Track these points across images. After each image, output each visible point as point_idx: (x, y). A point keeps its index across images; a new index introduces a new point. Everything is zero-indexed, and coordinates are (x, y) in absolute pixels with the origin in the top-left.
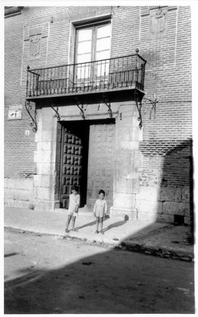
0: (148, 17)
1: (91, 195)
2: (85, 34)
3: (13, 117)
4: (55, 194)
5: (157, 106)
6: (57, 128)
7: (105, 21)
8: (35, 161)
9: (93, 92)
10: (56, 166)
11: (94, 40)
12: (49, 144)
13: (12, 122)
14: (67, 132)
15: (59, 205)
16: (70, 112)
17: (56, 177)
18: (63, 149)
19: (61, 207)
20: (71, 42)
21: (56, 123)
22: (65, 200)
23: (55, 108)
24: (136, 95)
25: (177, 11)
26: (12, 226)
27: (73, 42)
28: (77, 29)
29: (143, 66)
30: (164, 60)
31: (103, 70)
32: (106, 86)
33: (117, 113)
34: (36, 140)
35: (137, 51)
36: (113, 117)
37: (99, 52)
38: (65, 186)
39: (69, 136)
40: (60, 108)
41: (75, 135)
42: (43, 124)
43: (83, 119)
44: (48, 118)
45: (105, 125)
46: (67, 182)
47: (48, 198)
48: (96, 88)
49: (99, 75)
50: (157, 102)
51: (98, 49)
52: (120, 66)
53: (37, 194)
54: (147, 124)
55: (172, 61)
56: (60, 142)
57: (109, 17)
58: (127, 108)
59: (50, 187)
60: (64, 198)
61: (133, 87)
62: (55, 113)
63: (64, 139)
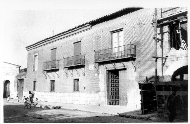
0: (136, 28)
1: (120, 99)
2: (115, 35)
3: (91, 69)
4: (107, 99)
5: (141, 63)
6: (107, 72)
7: (121, 30)
8: (99, 86)
9: (116, 59)
10: (107, 88)
11: (118, 37)
12: (104, 79)
13: (90, 71)
14: (111, 74)
15: (109, 104)
16: (111, 67)
17: (107, 92)
18: (110, 81)
19: (110, 104)
20: (110, 39)
21: (106, 71)
22: (112, 102)
23: (123, 63)
24: (132, 59)
25: (146, 25)
26: (87, 110)
27: (111, 38)
28: (112, 33)
29: (135, 47)
30: (142, 45)
31: (122, 49)
32: (121, 57)
33: (127, 66)
34: (99, 78)
35: (131, 43)
36: (126, 68)
37: (120, 42)
38: (111, 96)
39: (112, 75)
40: (107, 65)
41: (115, 75)
42: (101, 71)
43: (115, 69)
44: (103, 69)
45: (124, 71)
46: (112, 94)
47: (104, 101)
48: (117, 57)
49: (121, 51)
50: (141, 61)
51: (120, 41)
52: (127, 47)
53: (101, 99)
54: (138, 70)
55: (145, 45)
56: (108, 79)
57: (122, 29)
58: (129, 64)
59: (105, 96)
60: (111, 101)
61: (130, 57)
62: (123, 65)
63: (110, 77)
